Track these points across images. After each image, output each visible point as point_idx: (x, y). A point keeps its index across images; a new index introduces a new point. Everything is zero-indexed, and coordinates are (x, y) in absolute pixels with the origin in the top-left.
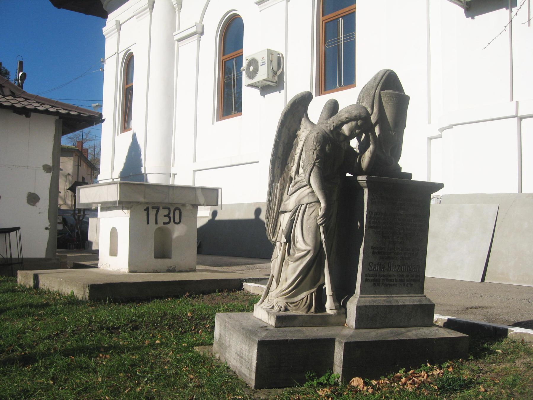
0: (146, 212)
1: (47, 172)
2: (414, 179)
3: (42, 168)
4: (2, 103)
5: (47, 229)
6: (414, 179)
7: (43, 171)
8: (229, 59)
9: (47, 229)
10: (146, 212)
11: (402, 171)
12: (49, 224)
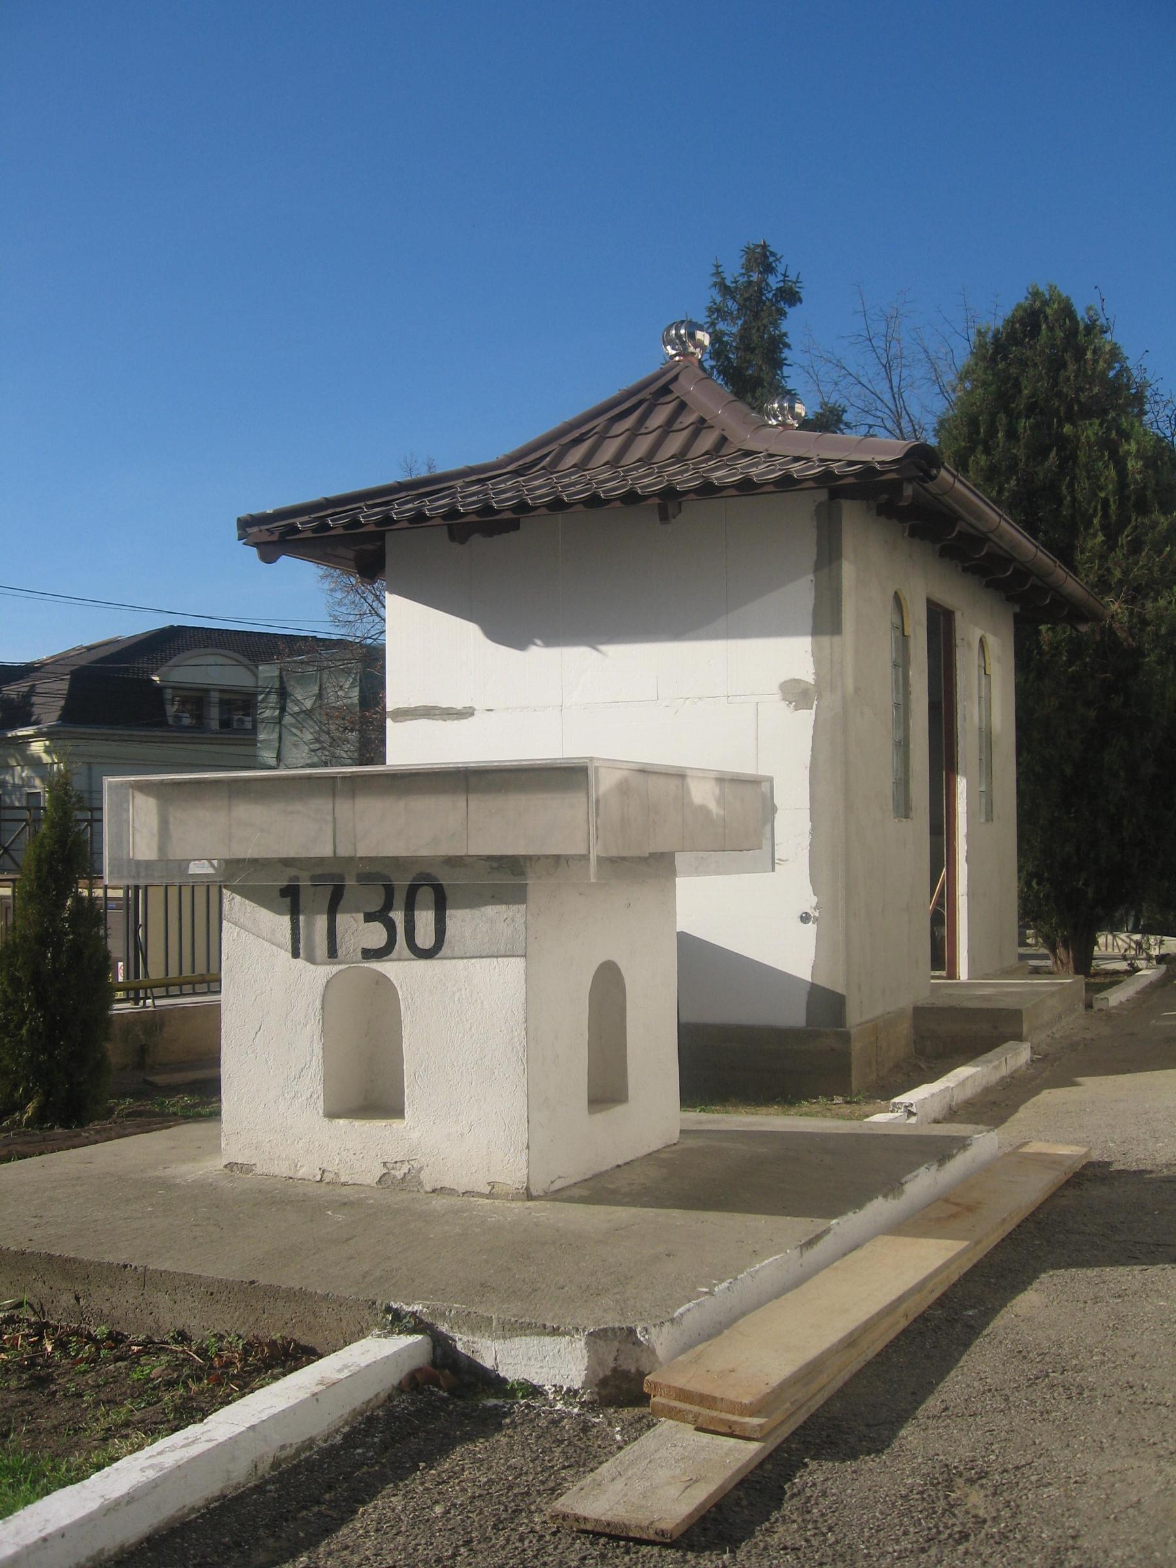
0: (288, 900)
1: (796, 708)
2: (880, 1198)
3: (778, 697)
4: (737, 493)
5: (805, 918)
6: (880, 1198)
7: (784, 704)
8: (129, 762)
9: (805, 918)
10: (288, 900)
11: (289, 898)
12: (814, 900)
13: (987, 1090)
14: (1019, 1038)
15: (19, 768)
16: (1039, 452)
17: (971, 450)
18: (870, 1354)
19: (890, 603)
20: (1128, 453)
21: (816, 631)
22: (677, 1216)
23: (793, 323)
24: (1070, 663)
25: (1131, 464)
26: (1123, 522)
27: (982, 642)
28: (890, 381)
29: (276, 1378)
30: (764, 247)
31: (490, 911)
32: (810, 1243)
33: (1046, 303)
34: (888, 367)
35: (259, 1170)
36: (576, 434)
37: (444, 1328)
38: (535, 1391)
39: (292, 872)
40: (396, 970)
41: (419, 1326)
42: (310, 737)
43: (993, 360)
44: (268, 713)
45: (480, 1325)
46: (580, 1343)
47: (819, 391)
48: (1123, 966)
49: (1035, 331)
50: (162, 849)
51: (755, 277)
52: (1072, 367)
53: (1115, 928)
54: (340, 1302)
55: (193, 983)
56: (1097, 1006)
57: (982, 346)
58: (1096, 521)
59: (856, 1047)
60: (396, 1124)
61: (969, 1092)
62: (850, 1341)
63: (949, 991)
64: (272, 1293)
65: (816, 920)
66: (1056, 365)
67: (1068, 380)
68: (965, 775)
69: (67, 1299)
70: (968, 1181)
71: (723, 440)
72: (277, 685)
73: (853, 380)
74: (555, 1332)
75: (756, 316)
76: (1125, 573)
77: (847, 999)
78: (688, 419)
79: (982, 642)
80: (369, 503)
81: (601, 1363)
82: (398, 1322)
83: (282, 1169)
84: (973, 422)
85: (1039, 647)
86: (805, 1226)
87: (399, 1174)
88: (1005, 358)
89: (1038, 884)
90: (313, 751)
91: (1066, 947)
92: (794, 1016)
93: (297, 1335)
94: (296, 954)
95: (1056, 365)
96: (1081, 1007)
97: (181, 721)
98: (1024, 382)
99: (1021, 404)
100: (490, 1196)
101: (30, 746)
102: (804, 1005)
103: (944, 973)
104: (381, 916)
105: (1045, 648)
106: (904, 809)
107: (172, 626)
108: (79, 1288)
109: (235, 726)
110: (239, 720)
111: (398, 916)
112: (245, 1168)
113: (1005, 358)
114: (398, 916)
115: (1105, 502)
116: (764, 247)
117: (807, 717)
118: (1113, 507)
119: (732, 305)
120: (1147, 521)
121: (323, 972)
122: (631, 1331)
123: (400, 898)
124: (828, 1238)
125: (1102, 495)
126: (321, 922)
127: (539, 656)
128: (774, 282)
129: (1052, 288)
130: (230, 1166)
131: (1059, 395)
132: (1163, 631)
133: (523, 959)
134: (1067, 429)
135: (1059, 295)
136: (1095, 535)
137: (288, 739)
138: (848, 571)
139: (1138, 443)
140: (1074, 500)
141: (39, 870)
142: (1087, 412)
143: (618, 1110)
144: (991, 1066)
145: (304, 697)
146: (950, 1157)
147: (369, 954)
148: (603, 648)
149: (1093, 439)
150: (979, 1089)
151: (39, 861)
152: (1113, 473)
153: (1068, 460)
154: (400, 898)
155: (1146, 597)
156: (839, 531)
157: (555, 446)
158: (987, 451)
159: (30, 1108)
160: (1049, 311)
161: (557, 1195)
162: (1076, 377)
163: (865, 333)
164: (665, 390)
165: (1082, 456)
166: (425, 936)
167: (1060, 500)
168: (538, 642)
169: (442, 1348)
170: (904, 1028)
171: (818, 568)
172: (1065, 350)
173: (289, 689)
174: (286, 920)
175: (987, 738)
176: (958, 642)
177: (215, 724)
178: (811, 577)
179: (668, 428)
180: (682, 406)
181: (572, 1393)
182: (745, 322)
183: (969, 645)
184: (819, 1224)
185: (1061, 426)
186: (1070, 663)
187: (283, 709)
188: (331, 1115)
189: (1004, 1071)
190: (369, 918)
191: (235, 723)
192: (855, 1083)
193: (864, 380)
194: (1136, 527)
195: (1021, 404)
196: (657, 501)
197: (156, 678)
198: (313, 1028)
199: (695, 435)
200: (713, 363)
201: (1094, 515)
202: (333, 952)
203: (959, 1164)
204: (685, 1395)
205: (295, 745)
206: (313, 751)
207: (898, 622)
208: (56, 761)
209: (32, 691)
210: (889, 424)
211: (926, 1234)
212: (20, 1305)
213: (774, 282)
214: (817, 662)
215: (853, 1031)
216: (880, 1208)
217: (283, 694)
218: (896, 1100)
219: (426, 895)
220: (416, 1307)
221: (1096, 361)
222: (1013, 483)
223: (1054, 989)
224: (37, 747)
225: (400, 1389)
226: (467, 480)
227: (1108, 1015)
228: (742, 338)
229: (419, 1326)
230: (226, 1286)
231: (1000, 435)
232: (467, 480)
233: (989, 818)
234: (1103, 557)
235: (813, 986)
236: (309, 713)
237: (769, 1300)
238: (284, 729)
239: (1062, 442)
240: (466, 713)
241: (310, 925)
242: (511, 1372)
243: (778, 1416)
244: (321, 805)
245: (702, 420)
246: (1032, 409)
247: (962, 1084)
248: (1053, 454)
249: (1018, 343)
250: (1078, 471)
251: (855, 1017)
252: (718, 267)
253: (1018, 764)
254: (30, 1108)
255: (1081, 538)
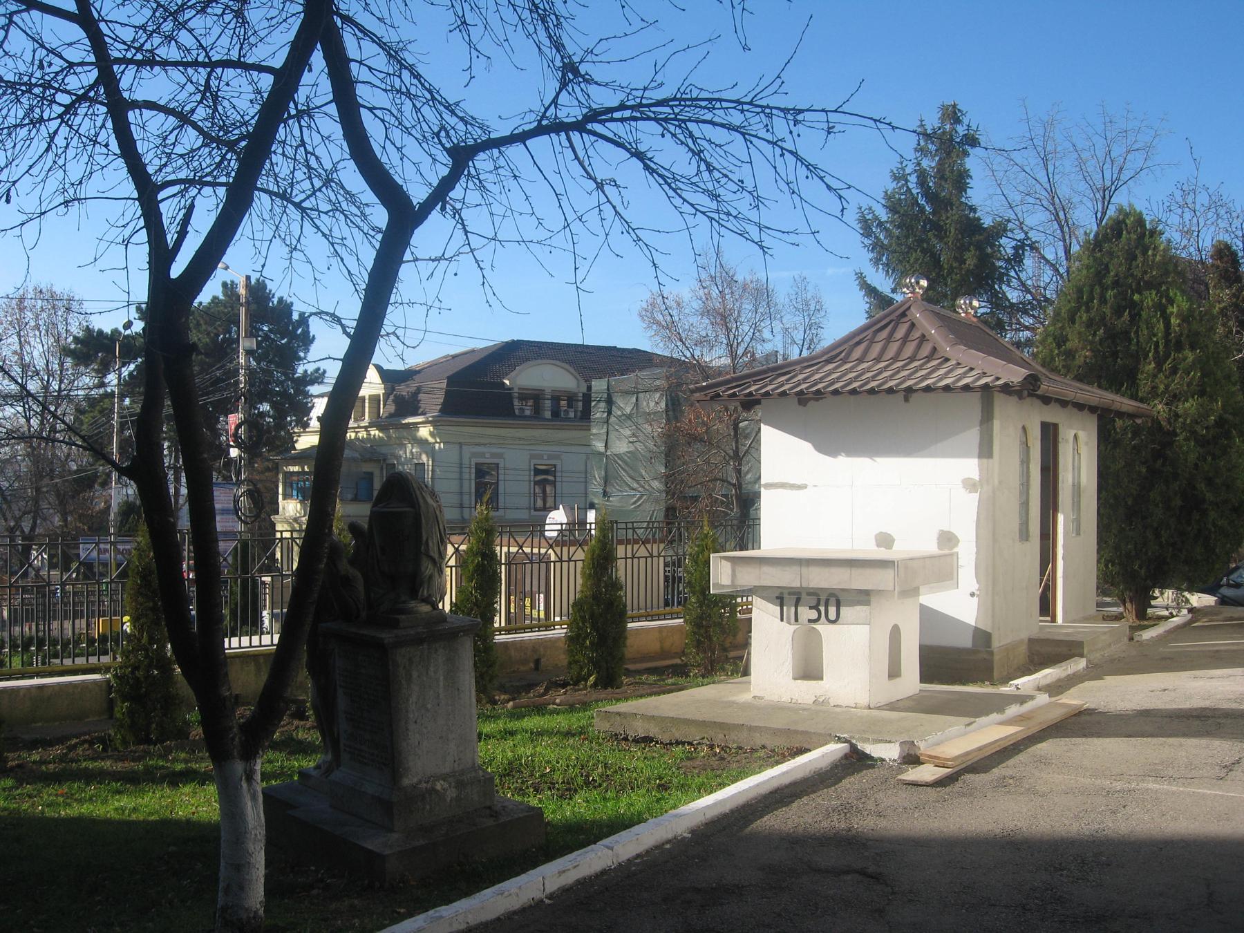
1: (970, 492)
5: (972, 595)
7: (964, 490)
9: (972, 595)
13: (1059, 680)
14: (1082, 656)
15: (410, 445)
16: (1118, 312)
17: (1078, 309)
18: (987, 754)
19: (1020, 431)
20: (1172, 313)
21: (980, 456)
22: (923, 716)
23: (973, 162)
24: (1133, 439)
25: (1173, 320)
26: (1167, 356)
27: (1076, 436)
28: (1047, 170)
29: (638, 856)
30: (954, 106)
31: (858, 608)
32: (969, 725)
33: (1127, 215)
34: (1045, 160)
35: (766, 698)
36: (857, 339)
37: (854, 742)
38: (882, 760)
39: (780, 590)
40: (823, 628)
41: (846, 741)
42: (629, 433)
43: (1094, 250)
44: (598, 415)
45: (866, 740)
46: (897, 745)
47: (994, 175)
48: (1166, 613)
49: (1119, 235)
50: (732, 581)
51: (948, 127)
52: (1140, 259)
53: (1163, 587)
54: (820, 735)
55: (652, 616)
56: (1135, 639)
57: (1088, 242)
58: (1150, 355)
59: (996, 658)
60: (820, 682)
61: (1048, 681)
62: (980, 749)
63: (1049, 630)
64: (796, 732)
65: (978, 596)
66: (1132, 257)
67: (1138, 267)
68: (1063, 513)
69: (721, 736)
70: (1032, 711)
71: (935, 349)
72: (605, 395)
73: (1020, 170)
74: (890, 742)
75: (949, 154)
76: (1167, 387)
77: (993, 636)
78: (916, 334)
79: (1076, 436)
80: (754, 379)
81: (904, 751)
82: (839, 740)
83: (775, 698)
84: (1080, 291)
85: (1115, 430)
86: (967, 720)
87: (821, 700)
88: (1100, 251)
89: (1112, 566)
90: (630, 442)
91: (1131, 602)
92: (966, 642)
93: (804, 745)
94: (782, 620)
95: (1132, 257)
96: (1126, 639)
97: (523, 412)
98: (1111, 267)
99: (1109, 280)
100: (855, 708)
101: (418, 430)
102: (971, 636)
103: (1049, 619)
104: (815, 607)
105: (1118, 430)
106: (1024, 535)
107: (513, 340)
108: (725, 732)
109: (562, 416)
110: (565, 411)
111: (822, 609)
112: (761, 698)
113: (1100, 251)
114: (822, 609)
115: (1157, 342)
116: (954, 106)
117: (975, 497)
118: (1161, 347)
119: (932, 148)
120: (1180, 356)
121: (793, 627)
122: (913, 742)
123: (822, 602)
124: (975, 724)
125: (1155, 339)
126: (793, 609)
127: (843, 461)
128: (961, 130)
129: (1130, 205)
130: (754, 697)
131: (1132, 275)
132: (1188, 421)
133: (868, 626)
134: (1136, 297)
135: (1135, 211)
136: (1150, 363)
137: (613, 435)
138: (997, 424)
139: (1178, 306)
140: (1138, 341)
141: (593, 564)
142: (1150, 285)
143: (898, 680)
144: (1062, 669)
145: (625, 405)
146: (1026, 702)
147: (810, 621)
148: (876, 459)
149: (1150, 304)
150: (1054, 680)
151: (593, 559)
152: (1162, 326)
153: (1135, 317)
154: (822, 602)
155: (1179, 400)
156: (992, 402)
157: (846, 346)
158: (1088, 310)
159: (592, 678)
160: (1127, 221)
161: (879, 708)
162: (1143, 265)
163: (1028, 135)
164: (904, 314)
165: (1144, 314)
166: (832, 616)
167: (1130, 340)
168: (843, 454)
169: (854, 748)
170: (1023, 649)
171: (982, 423)
172: (1137, 248)
173: (614, 399)
174: (779, 608)
175: (1077, 490)
176: (1060, 440)
177: (548, 414)
178: (978, 428)
179: (905, 340)
180: (913, 325)
181: (895, 760)
182: (940, 159)
183: (1067, 441)
184: (972, 720)
185: (1133, 294)
186: (1133, 439)
187: (609, 413)
188: (795, 679)
189: (1070, 671)
190: (811, 608)
191: (562, 413)
192: (996, 674)
193: (1027, 169)
194: (1174, 359)
195: (1109, 280)
196: (904, 393)
197: (507, 382)
198: (789, 646)
199: (919, 347)
200: (919, 191)
201: (1150, 351)
202: (796, 620)
203: (1029, 706)
204: (930, 756)
205: (619, 439)
206: (630, 442)
207: (1025, 440)
208: (438, 440)
209: (418, 391)
210: (1045, 203)
211: (1011, 725)
212: (703, 738)
213: (961, 130)
214: (980, 470)
215: (995, 650)
216: (995, 717)
217: (610, 402)
218: (1012, 682)
219: (833, 600)
220: (845, 736)
221: (1154, 255)
222: (1102, 331)
223: (1107, 630)
224: (424, 432)
225: (842, 758)
226: (803, 365)
227: (1141, 643)
228: (938, 170)
229: (846, 741)
230: (780, 730)
231: (1095, 301)
232: (803, 365)
233: (1078, 534)
234: (1155, 376)
235: (976, 630)
236: (629, 417)
237: (955, 738)
238: (610, 426)
239: (1133, 305)
240: (803, 487)
241: (788, 611)
242: (874, 755)
243: (957, 763)
244: (796, 569)
245: (923, 336)
246: (1116, 284)
247: (1046, 676)
248: (1126, 313)
249: (1110, 241)
250: (1141, 324)
251: (996, 644)
252: (922, 121)
253: (1099, 499)
254: (592, 678)
255: (1142, 364)
